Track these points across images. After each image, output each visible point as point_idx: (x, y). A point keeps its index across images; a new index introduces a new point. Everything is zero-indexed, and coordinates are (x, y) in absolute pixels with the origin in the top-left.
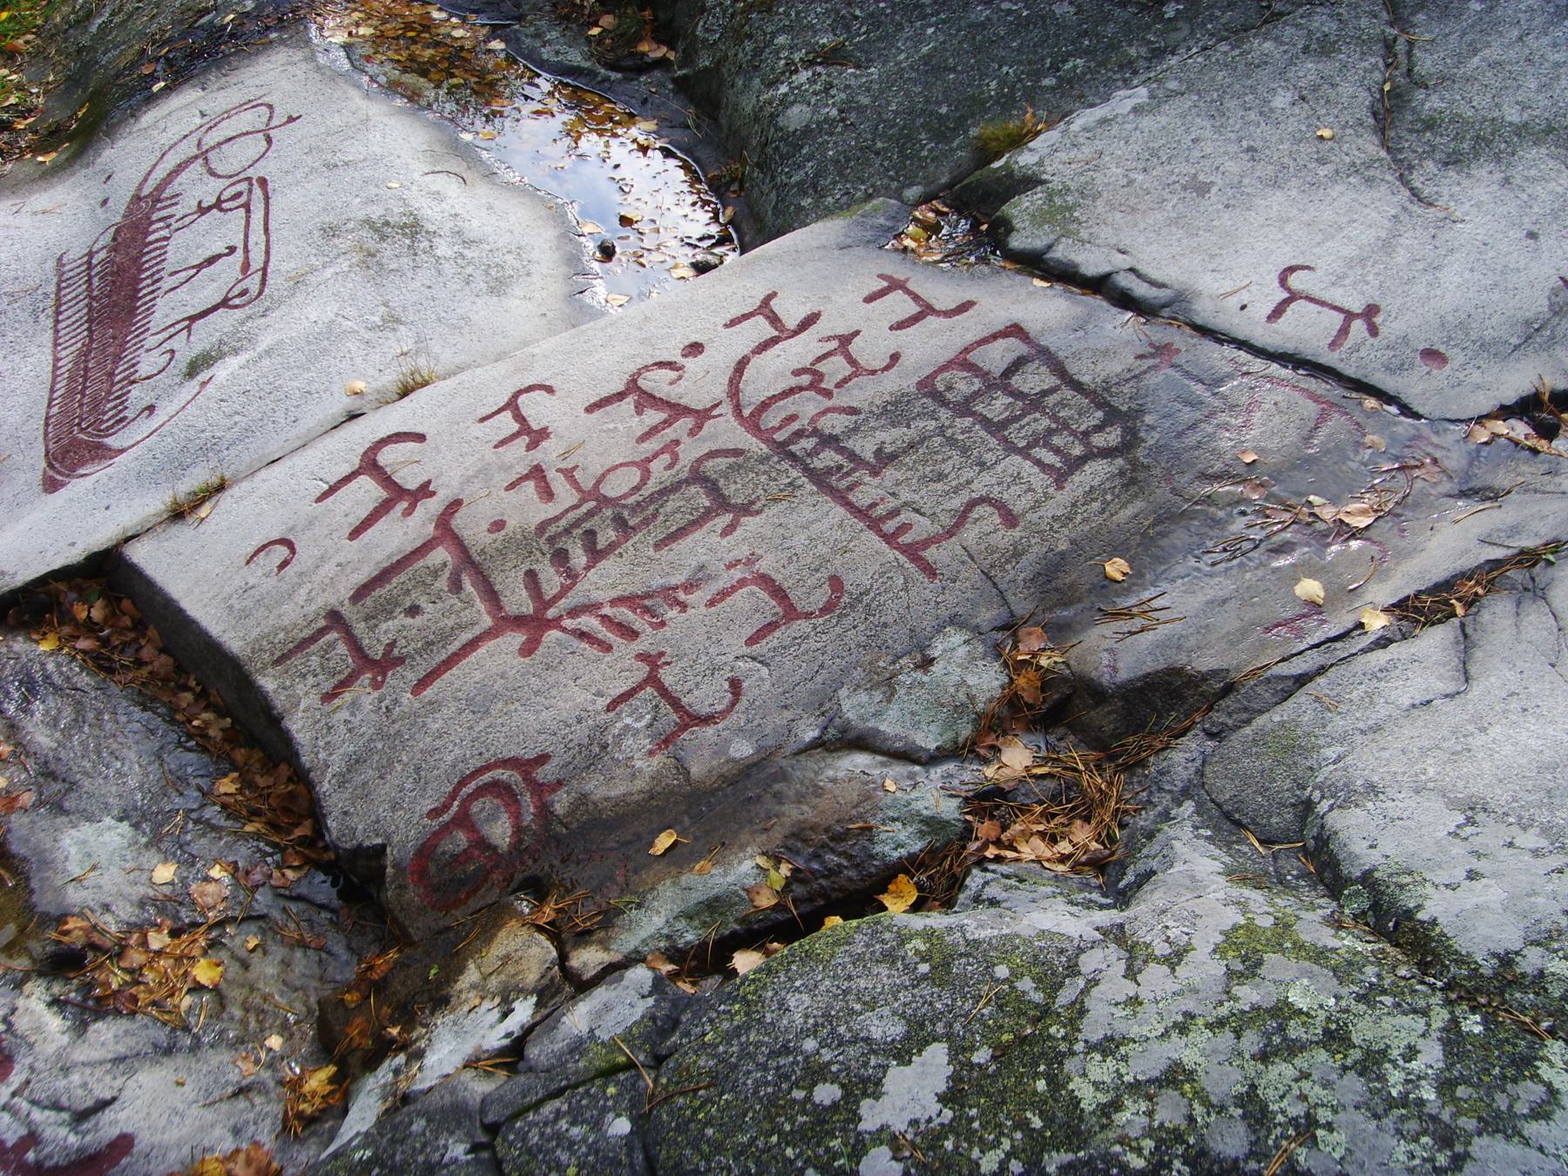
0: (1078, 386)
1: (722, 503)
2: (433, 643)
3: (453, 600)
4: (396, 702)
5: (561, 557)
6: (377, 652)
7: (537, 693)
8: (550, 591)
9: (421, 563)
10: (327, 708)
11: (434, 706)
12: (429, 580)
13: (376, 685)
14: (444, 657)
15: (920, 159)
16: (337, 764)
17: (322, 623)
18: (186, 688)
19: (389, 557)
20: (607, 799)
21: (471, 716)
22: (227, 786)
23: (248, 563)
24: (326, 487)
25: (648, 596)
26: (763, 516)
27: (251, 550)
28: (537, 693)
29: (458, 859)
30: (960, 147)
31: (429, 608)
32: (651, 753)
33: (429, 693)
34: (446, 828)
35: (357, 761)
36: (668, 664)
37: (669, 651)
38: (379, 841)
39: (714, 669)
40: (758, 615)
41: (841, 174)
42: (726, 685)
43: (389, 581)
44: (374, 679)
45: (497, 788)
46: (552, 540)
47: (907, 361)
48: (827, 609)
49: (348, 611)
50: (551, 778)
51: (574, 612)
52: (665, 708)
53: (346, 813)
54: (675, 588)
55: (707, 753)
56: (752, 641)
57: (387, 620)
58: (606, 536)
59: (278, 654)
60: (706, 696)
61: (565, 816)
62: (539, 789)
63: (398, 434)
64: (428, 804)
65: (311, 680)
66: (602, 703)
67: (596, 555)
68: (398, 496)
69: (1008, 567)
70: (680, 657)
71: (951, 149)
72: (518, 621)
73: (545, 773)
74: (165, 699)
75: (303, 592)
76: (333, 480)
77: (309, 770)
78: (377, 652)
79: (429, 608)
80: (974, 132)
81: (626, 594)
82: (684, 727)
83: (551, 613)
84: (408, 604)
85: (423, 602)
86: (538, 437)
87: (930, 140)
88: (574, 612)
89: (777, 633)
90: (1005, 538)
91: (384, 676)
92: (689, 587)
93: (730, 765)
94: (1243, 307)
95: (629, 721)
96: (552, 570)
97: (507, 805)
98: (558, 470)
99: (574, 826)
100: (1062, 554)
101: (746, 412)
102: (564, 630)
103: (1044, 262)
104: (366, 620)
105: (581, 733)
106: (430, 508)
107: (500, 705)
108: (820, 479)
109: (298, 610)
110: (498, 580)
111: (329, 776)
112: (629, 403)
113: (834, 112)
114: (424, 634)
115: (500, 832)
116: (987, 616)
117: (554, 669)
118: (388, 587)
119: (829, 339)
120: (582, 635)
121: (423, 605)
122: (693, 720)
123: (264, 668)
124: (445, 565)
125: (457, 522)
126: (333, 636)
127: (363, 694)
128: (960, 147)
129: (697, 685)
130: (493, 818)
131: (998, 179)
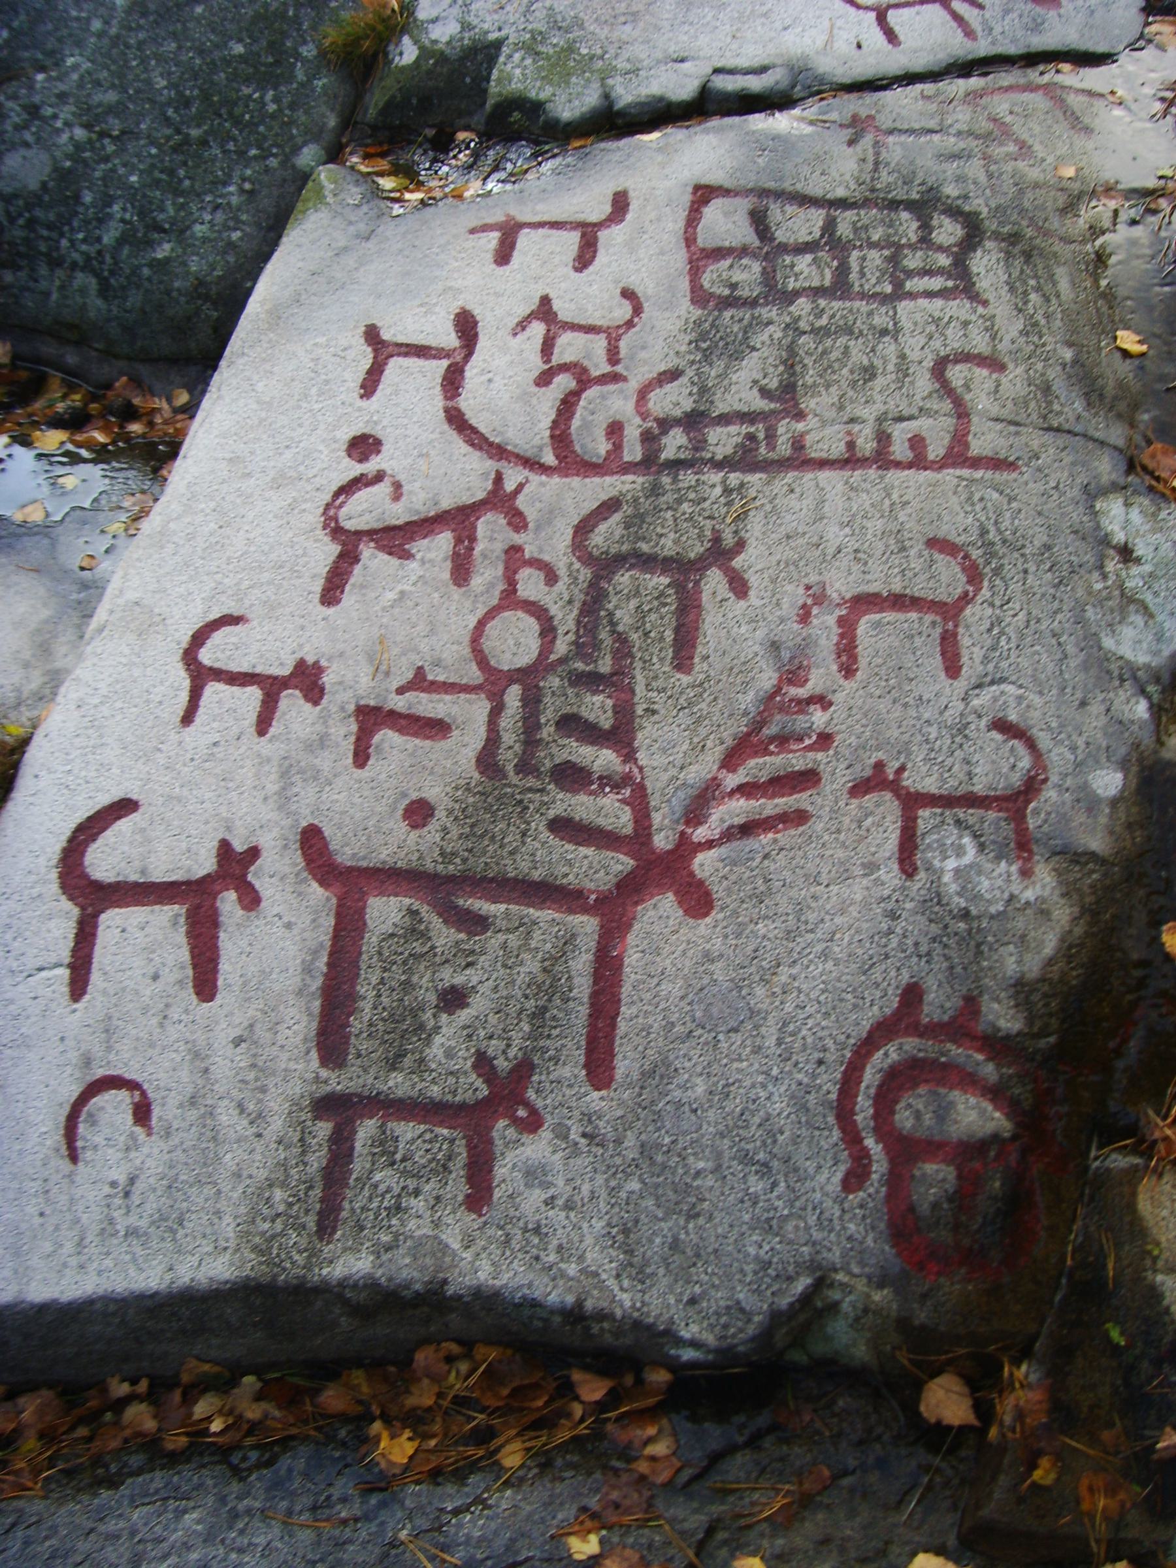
0: (843, 204)
1: (684, 572)
2: (541, 1012)
3: (494, 941)
4: (588, 1117)
5: (572, 776)
6: (474, 1087)
7: (790, 936)
8: (621, 819)
9: (371, 940)
10: (494, 1213)
11: (658, 1073)
12: (418, 947)
13: (533, 1124)
14: (584, 1010)
15: (273, 116)
16: (601, 1259)
17: (324, 1129)
18: (121, 1404)
19: (307, 970)
20: (1050, 962)
21: (737, 1038)
22: (396, 1449)
23: (74, 1157)
24: (64, 973)
25: (758, 724)
26: (752, 543)
27: (57, 1138)
28: (790, 936)
29: (962, 1197)
30: (311, 78)
31: (472, 976)
32: (1026, 873)
33: (625, 1064)
34: (896, 1180)
35: (626, 1231)
36: (902, 769)
37: (880, 755)
38: (802, 1284)
39: (962, 729)
40: (918, 641)
41: (178, 193)
42: (997, 736)
43: (353, 997)
44: (516, 1122)
45: (896, 1081)
46: (525, 767)
47: (646, 287)
48: (974, 575)
49: (337, 1082)
50: (954, 1003)
51: (695, 813)
52: (971, 815)
53: (693, 1301)
54: (778, 690)
55: (1081, 817)
56: (953, 669)
57: (428, 1041)
58: (597, 707)
59: (311, 1221)
60: (994, 765)
61: (1030, 1020)
62: (963, 1025)
63: (80, 829)
64: (831, 1178)
65: (418, 1204)
66: (890, 874)
67: (620, 735)
68: (206, 899)
69: (1056, 407)
70: (905, 749)
71: (302, 85)
72: (631, 889)
73: (938, 1002)
74: (114, 1444)
75: (226, 1116)
76: (65, 956)
77: (580, 1304)
78: (474, 1087)
79: (472, 976)
80: (308, 51)
81: (729, 742)
82: (1018, 817)
83: (662, 841)
84: (432, 998)
85: (449, 977)
86: (308, 679)
87: (263, 89)
88: (695, 813)
89: (965, 641)
90: (1014, 381)
91: (527, 1104)
92: (794, 674)
93: (1122, 807)
94: (859, 46)
95: (951, 864)
96: (583, 798)
97: (941, 1082)
98: (401, 691)
99: (1054, 1023)
100: (1075, 362)
101: (549, 459)
102: (710, 844)
103: (621, 113)
104: (393, 1068)
105: (914, 925)
106: (278, 873)
107: (760, 991)
108: (745, 459)
109: (259, 1146)
110: (520, 867)
111: (611, 1283)
112: (372, 558)
113: (80, 133)
114: (513, 1011)
115: (974, 1115)
116: (1106, 467)
117: (769, 892)
118: (366, 1006)
119: (522, 325)
120: (747, 829)
121: (459, 980)
122: (1017, 801)
123: (313, 1253)
124: (413, 913)
125: (347, 849)
126: (366, 1130)
127: (518, 1155)
128: (311, 78)
129: (966, 761)
130: (943, 1112)
131: (429, 72)
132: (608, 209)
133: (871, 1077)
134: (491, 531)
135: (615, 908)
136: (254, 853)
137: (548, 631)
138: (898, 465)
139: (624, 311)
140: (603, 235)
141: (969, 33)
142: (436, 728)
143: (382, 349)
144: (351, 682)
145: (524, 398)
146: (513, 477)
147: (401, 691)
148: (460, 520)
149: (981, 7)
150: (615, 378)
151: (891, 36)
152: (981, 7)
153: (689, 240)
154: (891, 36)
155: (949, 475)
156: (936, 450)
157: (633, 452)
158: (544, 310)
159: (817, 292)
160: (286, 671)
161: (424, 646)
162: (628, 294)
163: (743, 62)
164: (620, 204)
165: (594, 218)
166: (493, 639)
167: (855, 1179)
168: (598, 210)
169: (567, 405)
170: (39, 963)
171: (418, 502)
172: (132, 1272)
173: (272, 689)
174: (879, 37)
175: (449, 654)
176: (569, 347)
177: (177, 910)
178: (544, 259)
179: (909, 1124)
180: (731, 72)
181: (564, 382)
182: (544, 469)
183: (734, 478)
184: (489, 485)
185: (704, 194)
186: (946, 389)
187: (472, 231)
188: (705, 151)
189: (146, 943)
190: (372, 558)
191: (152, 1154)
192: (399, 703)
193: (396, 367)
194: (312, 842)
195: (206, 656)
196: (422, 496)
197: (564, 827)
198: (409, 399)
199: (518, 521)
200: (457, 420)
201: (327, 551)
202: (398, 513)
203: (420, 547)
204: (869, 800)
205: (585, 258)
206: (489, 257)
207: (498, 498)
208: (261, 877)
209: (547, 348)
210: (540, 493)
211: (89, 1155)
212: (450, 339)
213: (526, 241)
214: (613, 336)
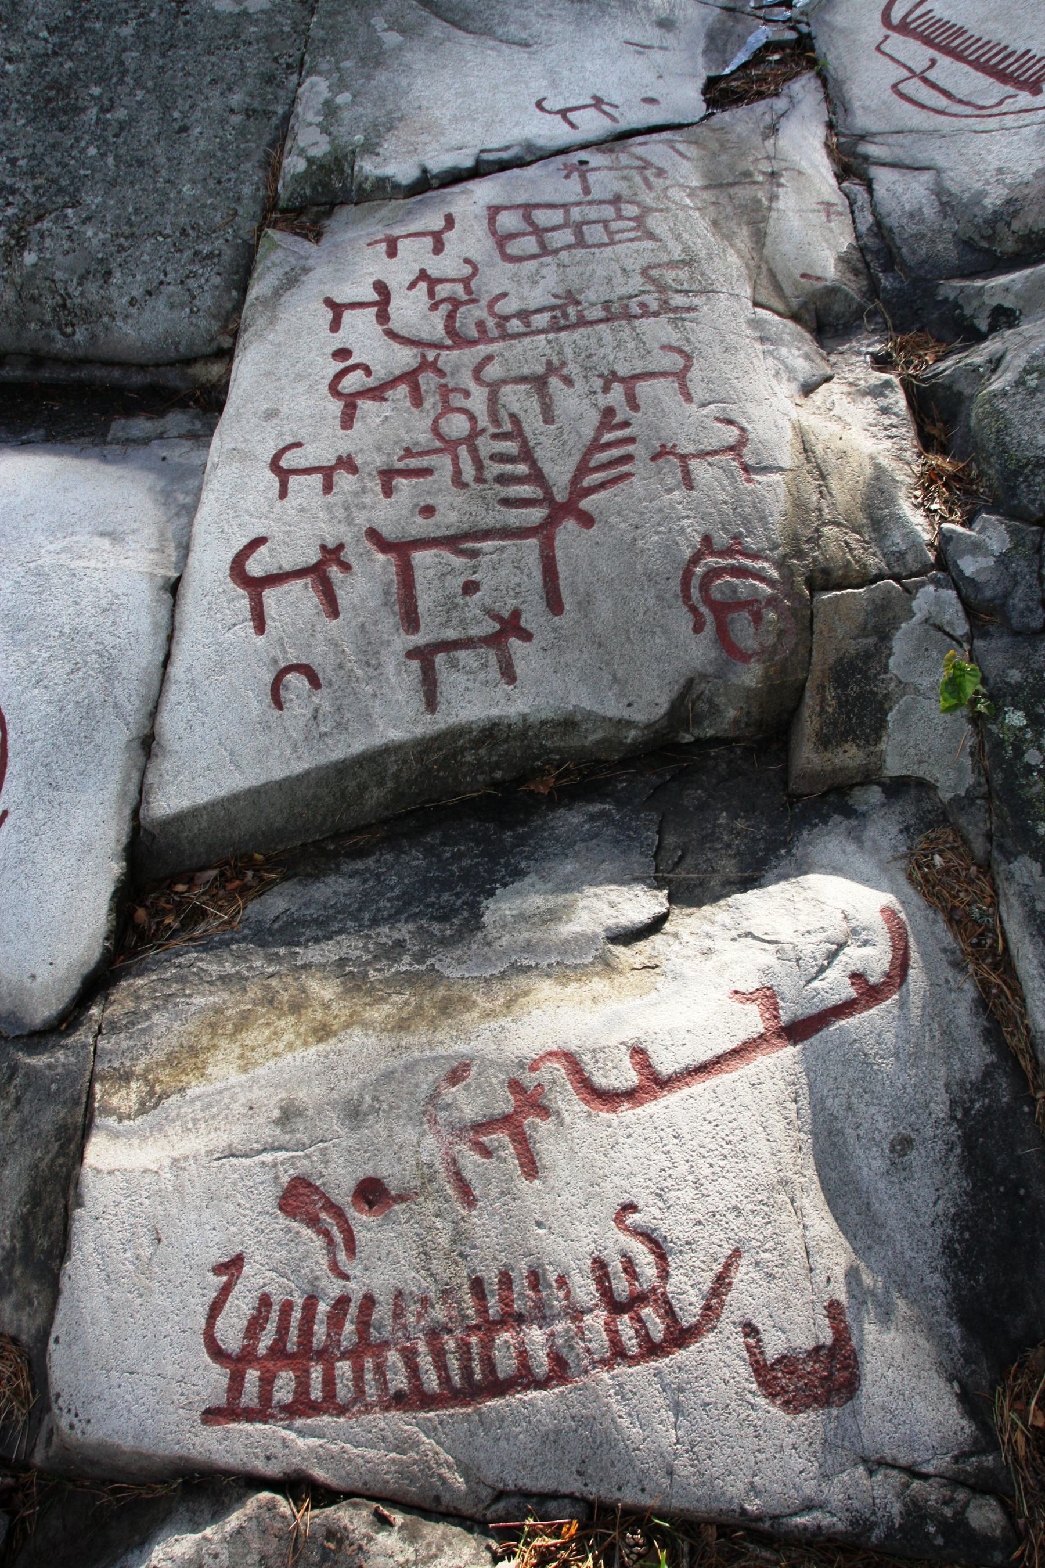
46: (480, 479)
49: (419, 639)
68: (323, 571)
78: (491, 627)
86: (347, 464)
112: (365, 405)
126: (440, 659)
132: (443, 223)
133: (695, 582)
134: (427, 381)
135: (545, 532)
136: (341, 547)
137: (472, 418)
138: (636, 317)
139: (468, 270)
140: (445, 236)
141: (614, 119)
142: (426, 472)
143: (337, 309)
144: (371, 460)
145: (425, 317)
146: (431, 355)
147: (400, 459)
148: (410, 377)
149: (5, 813)
150: (474, 301)
151: (572, 125)
152: (5, 813)
153: (494, 233)
154: (572, 125)
155: (663, 319)
156: (654, 306)
157: (494, 333)
158: (423, 275)
159: (569, 247)
160: (333, 462)
161: (407, 438)
162: (467, 261)
163: (495, 146)
164: (449, 221)
165: (436, 229)
166: (444, 427)
167: (698, 628)
168: (438, 224)
169: (451, 317)
170: (233, 621)
171: (380, 374)
172: (328, 753)
173: (327, 473)
174: (566, 127)
175: (423, 437)
176: (443, 291)
177: (308, 580)
178: (415, 254)
179: (719, 596)
180: (490, 151)
181: (445, 308)
182: (448, 348)
183: (551, 336)
184: (419, 360)
185: (494, 211)
186: (653, 281)
187: (369, 245)
188: (484, 191)
189: (292, 605)
190: (365, 405)
191: (322, 699)
192: (400, 465)
193: (347, 316)
194: (373, 534)
195: (283, 464)
196: (383, 371)
197: (506, 502)
198: (361, 331)
199: (441, 373)
200: (391, 334)
201: (336, 407)
202: (371, 382)
203: (389, 394)
204: (661, 461)
205: (438, 248)
206: (384, 256)
207: (424, 365)
208: (349, 555)
209: (431, 294)
210: (448, 358)
211: (288, 705)
212: (374, 297)
213: (401, 245)
214: (466, 281)
